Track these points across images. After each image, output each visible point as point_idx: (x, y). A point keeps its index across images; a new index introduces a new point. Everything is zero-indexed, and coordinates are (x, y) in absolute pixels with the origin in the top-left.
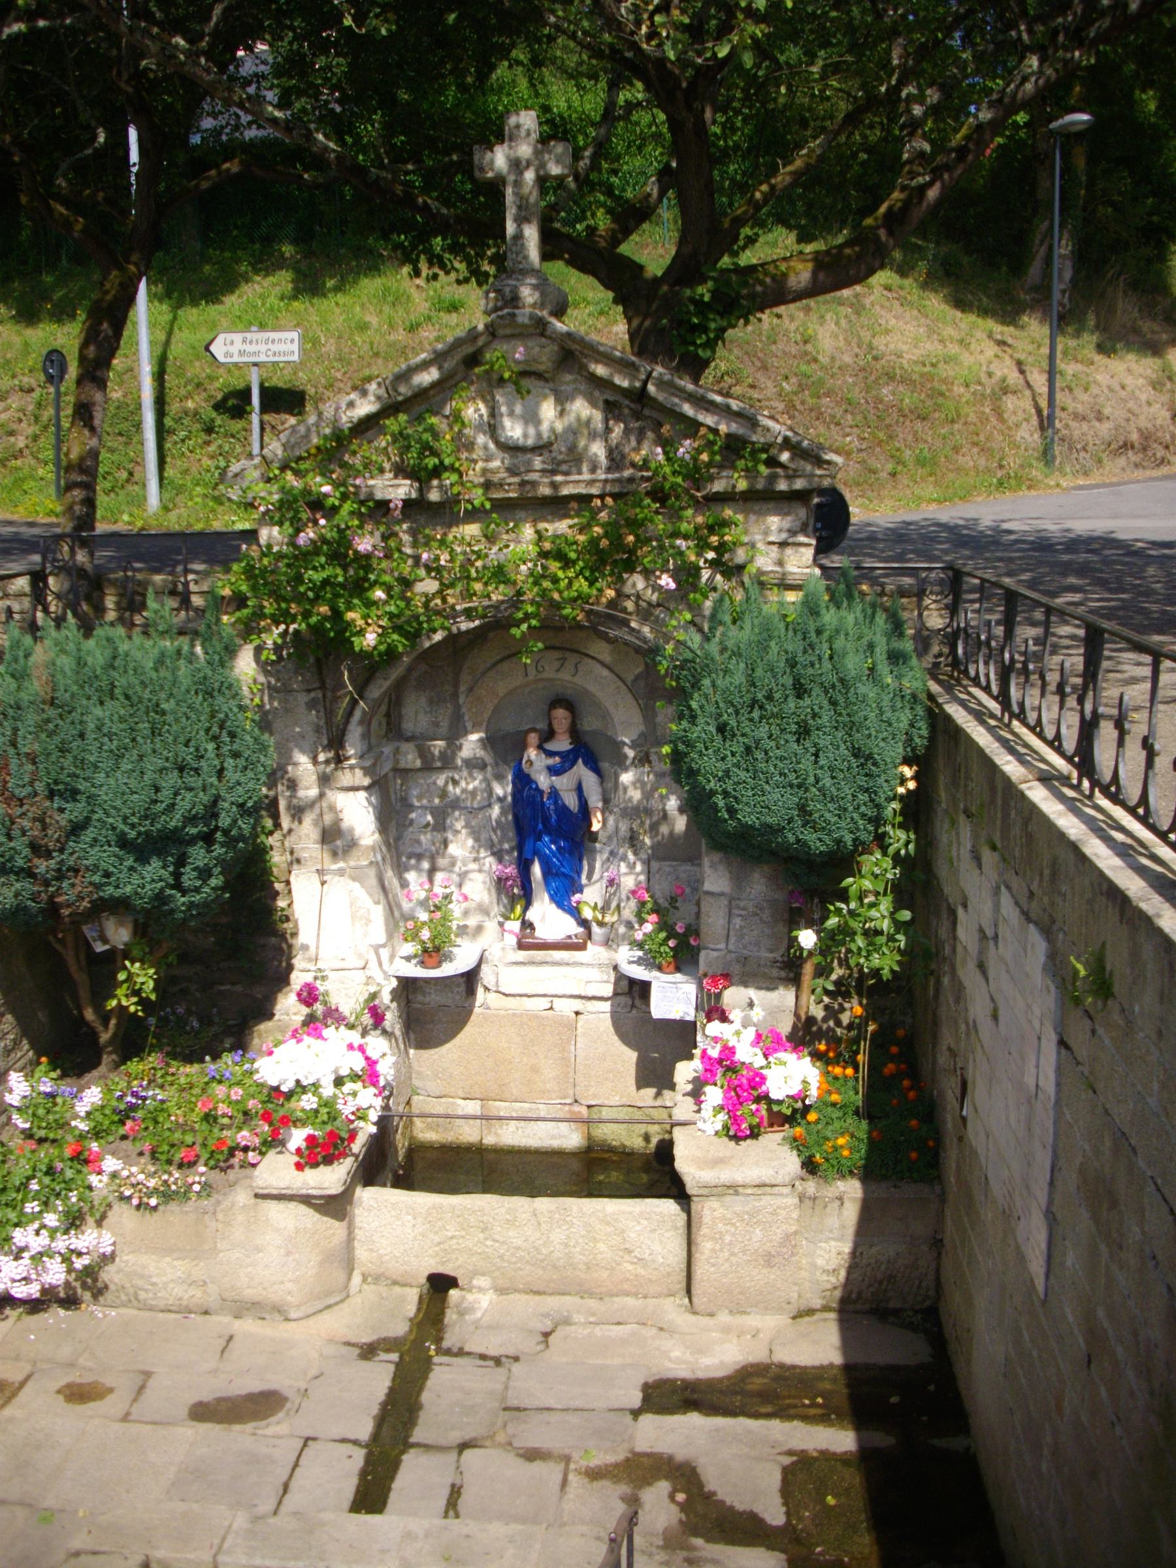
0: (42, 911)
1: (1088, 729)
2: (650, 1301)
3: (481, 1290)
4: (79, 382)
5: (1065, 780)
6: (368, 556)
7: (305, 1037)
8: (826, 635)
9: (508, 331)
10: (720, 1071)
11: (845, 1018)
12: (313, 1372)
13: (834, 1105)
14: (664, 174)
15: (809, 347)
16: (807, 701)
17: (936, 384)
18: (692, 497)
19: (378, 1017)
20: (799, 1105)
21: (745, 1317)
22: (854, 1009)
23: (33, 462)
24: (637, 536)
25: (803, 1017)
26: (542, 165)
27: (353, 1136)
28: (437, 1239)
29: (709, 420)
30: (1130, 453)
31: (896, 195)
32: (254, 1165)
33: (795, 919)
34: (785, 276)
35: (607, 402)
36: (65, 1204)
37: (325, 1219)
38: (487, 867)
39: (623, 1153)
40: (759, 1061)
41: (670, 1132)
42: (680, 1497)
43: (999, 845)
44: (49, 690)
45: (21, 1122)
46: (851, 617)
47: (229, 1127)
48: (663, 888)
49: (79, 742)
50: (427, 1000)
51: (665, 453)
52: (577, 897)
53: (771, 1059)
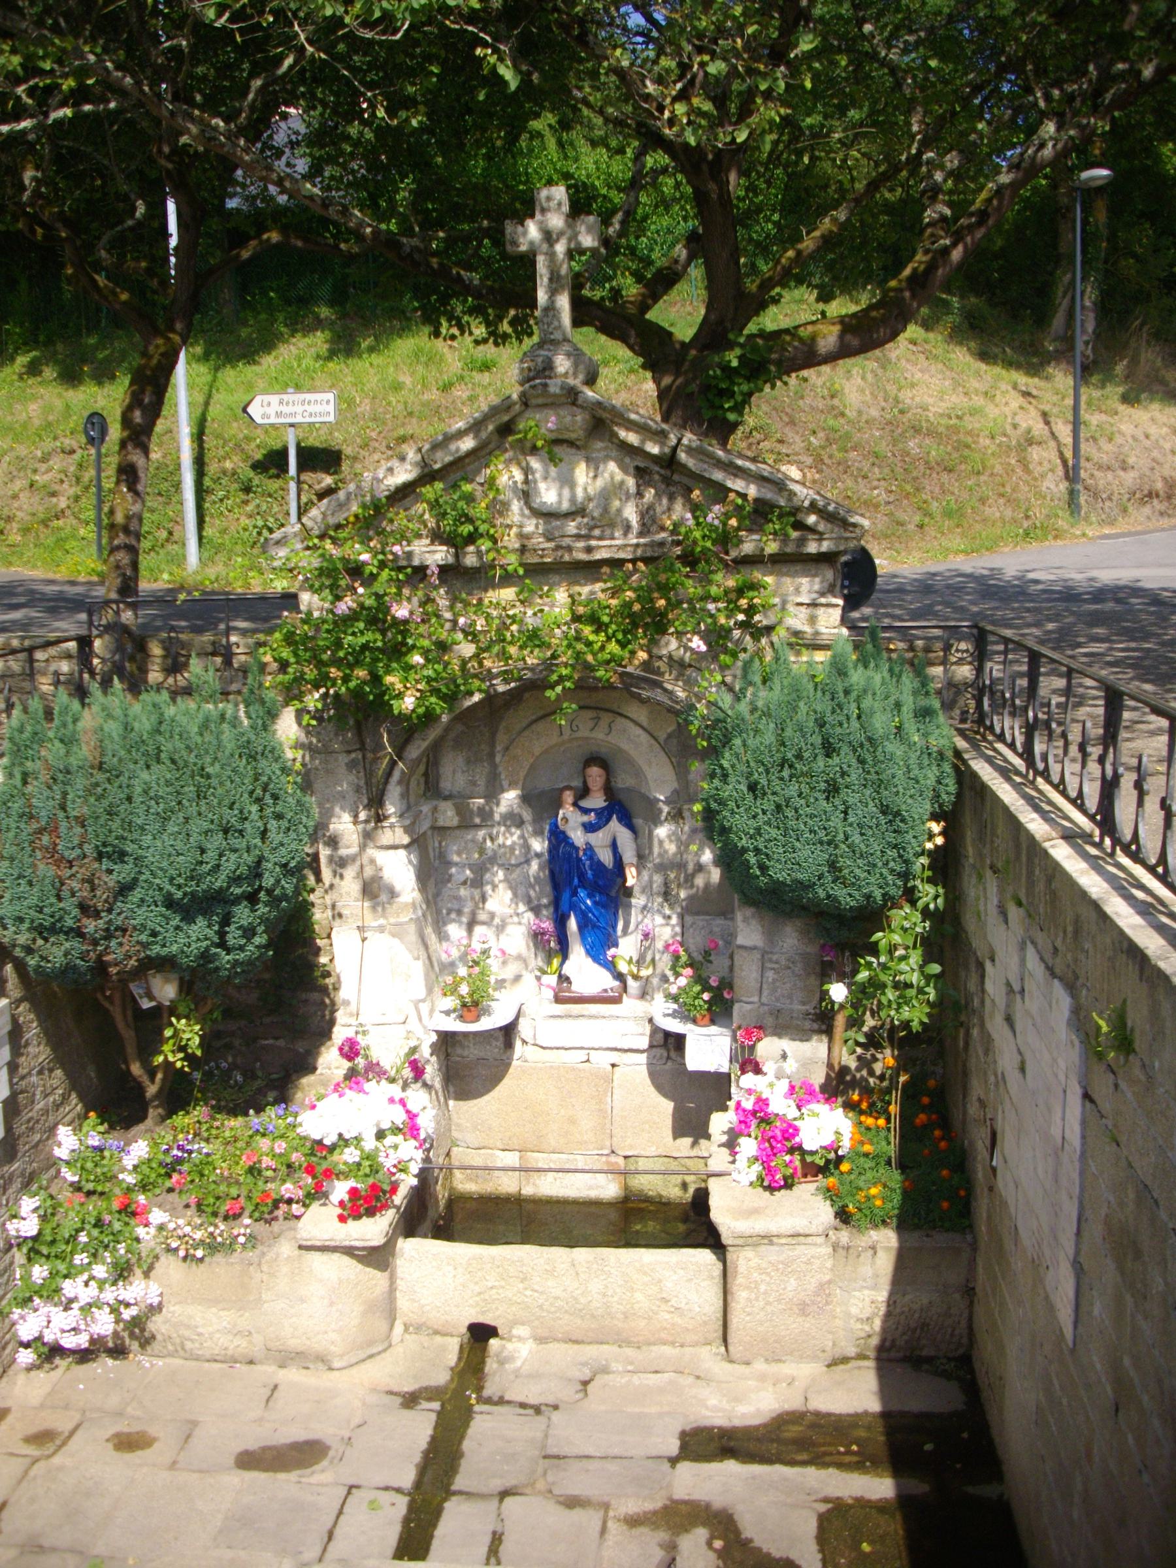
0: (91, 969)
1: (1109, 788)
2: (687, 1350)
3: (520, 1339)
4: (123, 444)
5: (1087, 837)
6: (406, 622)
7: (347, 1091)
8: (854, 695)
9: (540, 401)
10: (754, 1123)
11: (878, 1068)
12: (356, 1420)
13: (866, 1155)
14: (692, 239)
15: (836, 402)
16: (836, 760)
17: (961, 436)
18: (721, 560)
19: (418, 1071)
20: (832, 1156)
21: (781, 1365)
22: (886, 1059)
23: (74, 522)
24: (668, 600)
25: (837, 1068)
26: (574, 237)
27: (394, 1189)
28: (477, 1289)
29: (738, 485)
30: (1155, 501)
31: (919, 257)
32: (298, 1217)
33: (826, 972)
34: (813, 338)
35: (637, 468)
36: (113, 1256)
37: (368, 1269)
38: (525, 921)
39: (660, 1203)
40: (791, 1112)
41: (705, 1181)
42: (718, 1544)
43: (1024, 901)
44: (97, 755)
45: (70, 1176)
46: (878, 677)
47: (273, 1180)
48: (697, 941)
49: (126, 805)
50: (466, 1053)
51: (695, 518)
52: (612, 951)
53: (804, 1110)
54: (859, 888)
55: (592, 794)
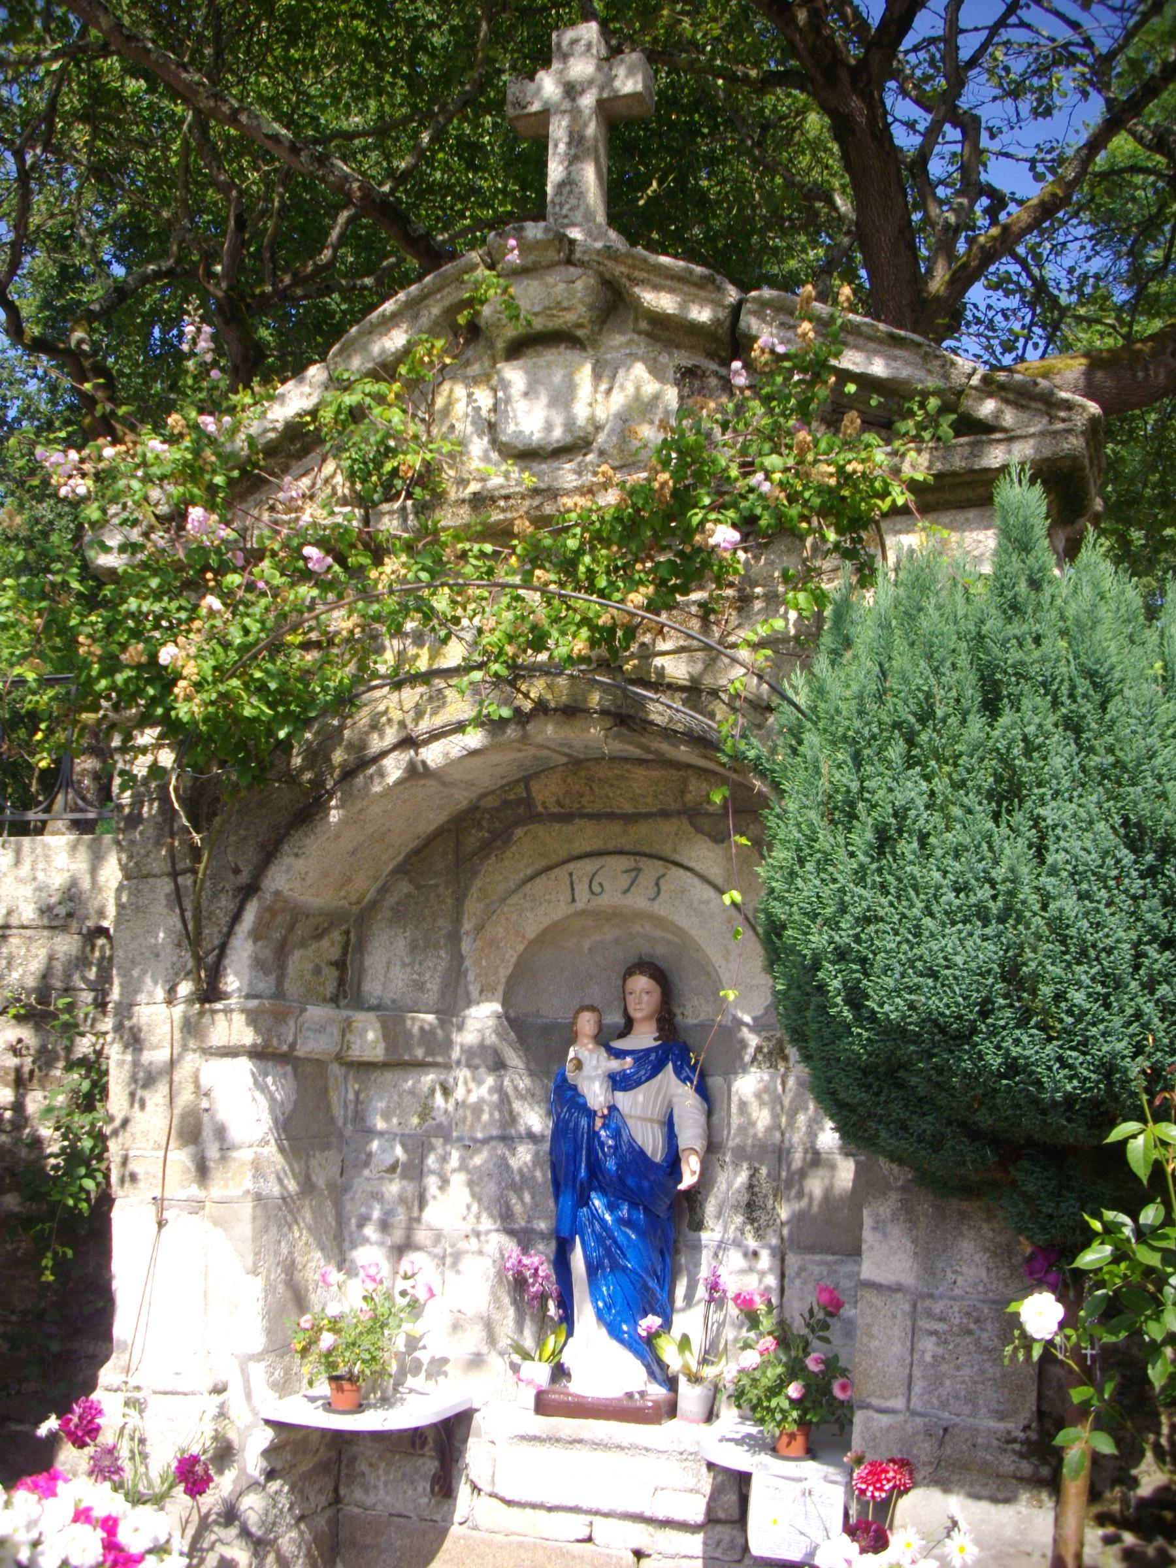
50: (370, 1500)
54: (1083, 1046)
55: (637, 1027)
